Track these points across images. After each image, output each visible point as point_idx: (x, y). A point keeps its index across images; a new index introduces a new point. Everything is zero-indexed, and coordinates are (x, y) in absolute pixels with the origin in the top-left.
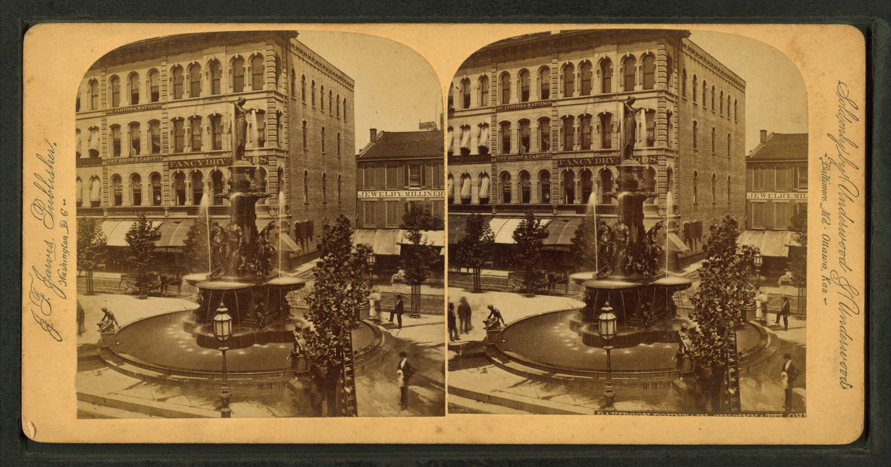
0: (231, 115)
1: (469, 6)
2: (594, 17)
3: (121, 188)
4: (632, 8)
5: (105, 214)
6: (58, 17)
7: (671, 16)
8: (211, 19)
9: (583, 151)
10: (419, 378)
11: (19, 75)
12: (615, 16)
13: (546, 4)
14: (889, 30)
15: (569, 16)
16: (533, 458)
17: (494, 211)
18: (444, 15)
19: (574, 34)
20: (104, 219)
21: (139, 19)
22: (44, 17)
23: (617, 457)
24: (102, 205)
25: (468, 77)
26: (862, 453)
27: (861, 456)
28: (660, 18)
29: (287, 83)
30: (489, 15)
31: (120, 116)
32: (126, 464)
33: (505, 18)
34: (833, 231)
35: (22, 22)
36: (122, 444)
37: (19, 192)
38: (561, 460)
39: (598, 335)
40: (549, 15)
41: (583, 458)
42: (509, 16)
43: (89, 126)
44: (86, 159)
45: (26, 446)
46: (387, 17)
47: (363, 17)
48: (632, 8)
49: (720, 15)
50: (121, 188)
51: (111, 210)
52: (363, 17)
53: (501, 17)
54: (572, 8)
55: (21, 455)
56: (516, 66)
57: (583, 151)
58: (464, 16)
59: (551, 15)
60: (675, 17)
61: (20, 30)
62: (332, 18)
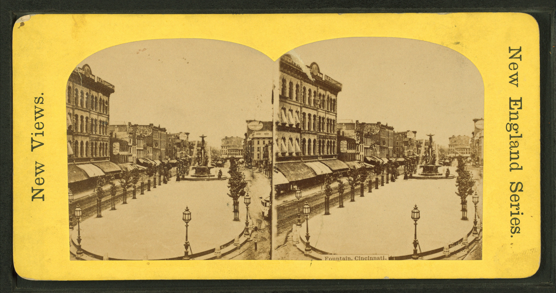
0: (284, 201)
4: (400, 2)
7: (425, 8)
10: (263, 231)
14: (113, 144)
15: (360, 8)
16: (339, 289)
21: (87, 11)
22: (27, 10)
23: (392, 288)
25: (113, 181)
26: (548, 285)
27: (548, 287)
33: (320, 9)
34: (390, 134)
35: (13, 14)
37: (11, 122)
38: (357, 291)
40: (348, 8)
41: (371, 290)
42: (322, 9)
45: (17, 283)
55: (13, 289)
58: (293, 8)
59: (348, 8)
60: (428, 9)
61: (11, 20)
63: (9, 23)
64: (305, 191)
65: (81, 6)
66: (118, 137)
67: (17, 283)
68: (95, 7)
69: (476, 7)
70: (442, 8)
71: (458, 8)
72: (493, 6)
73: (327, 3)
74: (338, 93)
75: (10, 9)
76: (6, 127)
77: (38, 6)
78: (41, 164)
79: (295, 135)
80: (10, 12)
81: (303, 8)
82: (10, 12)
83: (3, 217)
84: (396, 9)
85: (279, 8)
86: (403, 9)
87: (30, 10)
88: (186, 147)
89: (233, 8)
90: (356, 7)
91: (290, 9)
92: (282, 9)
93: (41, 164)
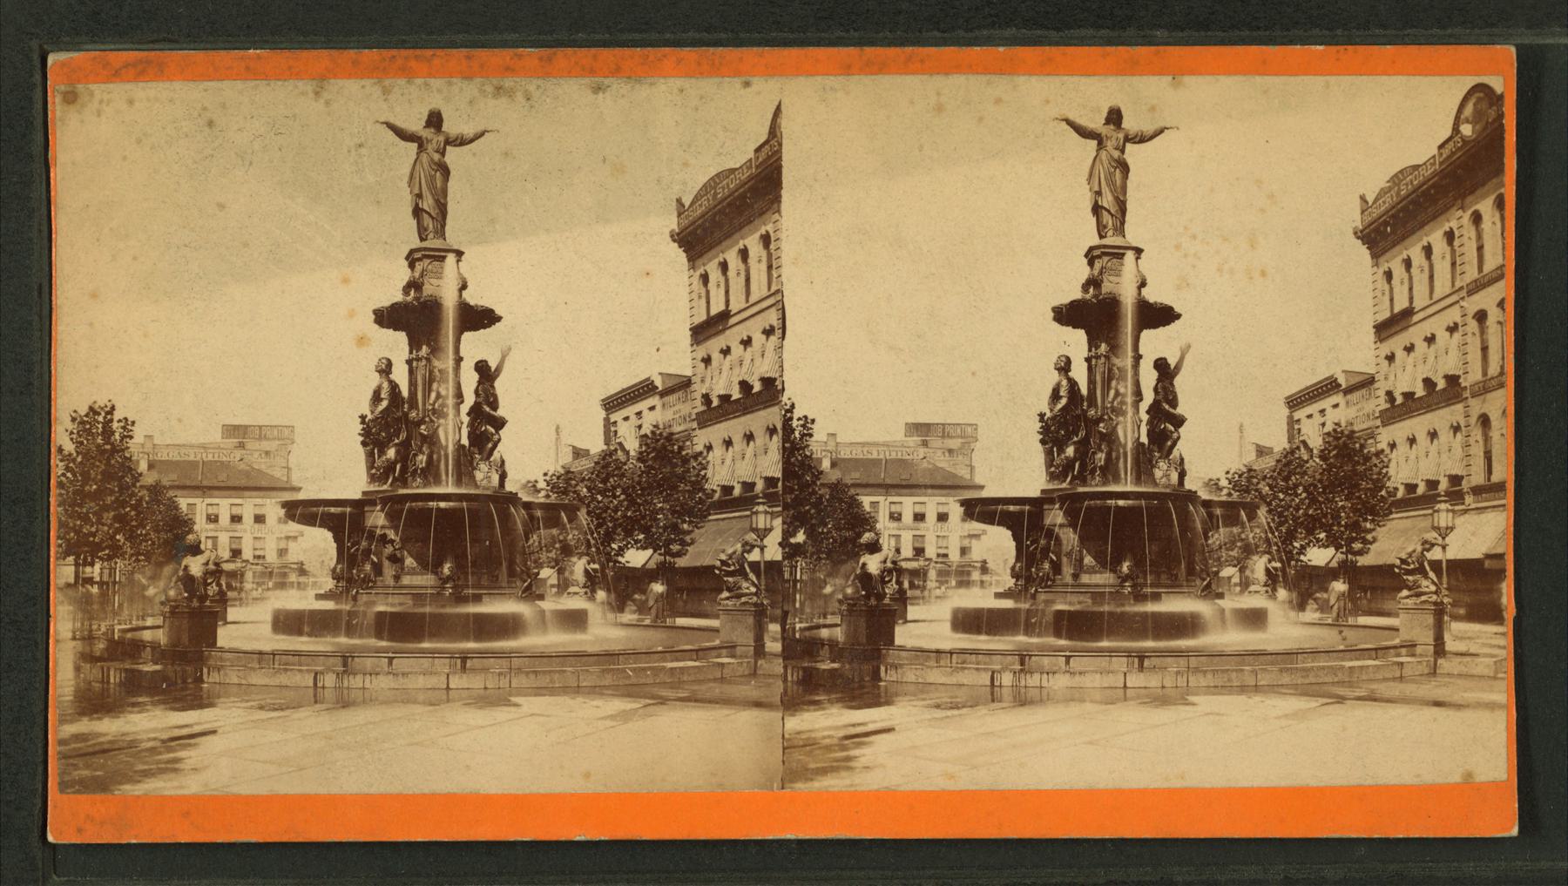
2: (1142, 34)
4: (1213, 13)
5: (1469, 499)
6: (110, 39)
7: (1288, 30)
8: (404, 42)
9: (1122, 251)
11: (37, 149)
17: (1469, 499)
19: (89, 47)
20: (1466, 511)
24: (1465, 485)
29: (695, 674)
30: (938, 30)
32: (1020, 884)
33: (970, 35)
36: (482, 842)
39: (1318, 595)
40: (1054, 29)
46: (742, 35)
47: (697, 36)
48: (1213, 13)
49: (1384, 27)
51: (1477, 491)
52: (697, 36)
53: (961, 33)
54: (1098, 16)
56: (1484, 197)
57: (1122, 251)
59: (1058, 29)
62: (637, 36)
63: (32, 76)
64: (793, 715)
65: (248, 27)
66: (71, 608)
67: (54, 865)
68: (290, 29)
69: (1444, 28)
70: (1339, 32)
72: (1493, 25)
73: (991, 16)
74: (330, 529)
75: (32, 34)
77: (117, 24)
78: (1416, 323)
79: (1442, 418)
80: (34, 44)
81: (920, 32)
82: (34, 44)
83: (13, 663)
84: (1203, 33)
85: (848, 31)
86: (1223, 34)
87: (93, 37)
88: (1452, 415)
89: (707, 30)
90: (1079, 27)
92: (856, 34)
93: (1416, 323)
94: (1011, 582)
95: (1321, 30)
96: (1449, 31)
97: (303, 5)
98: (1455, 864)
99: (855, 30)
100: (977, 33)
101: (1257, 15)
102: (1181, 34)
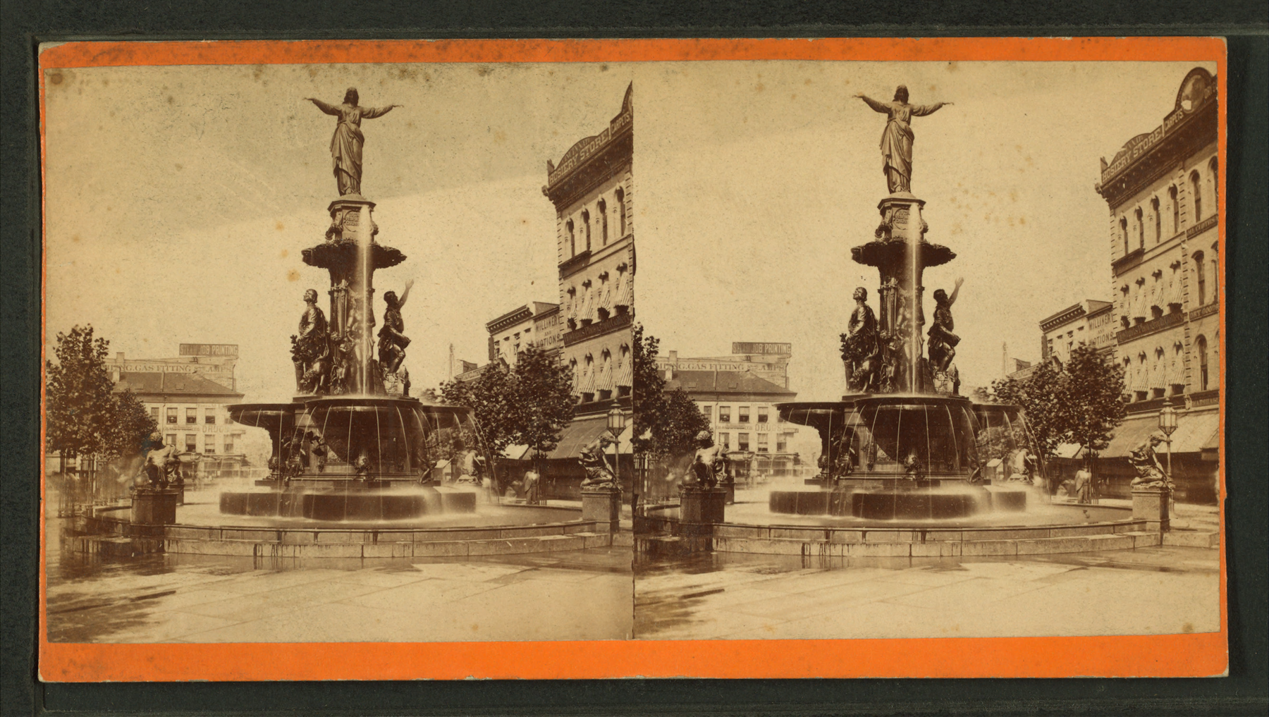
1: (728, 10)
3: (106, 351)
4: (982, 11)
5: (1189, 404)
7: (1042, 24)
8: (327, 34)
9: (908, 203)
12: (957, 24)
13: (803, 10)
15: (883, 26)
18: (689, 25)
21: (215, 34)
28: (438, 30)
30: (759, 24)
31: (1200, 237)
40: (853, 23)
43: (1170, 263)
44: (598, 323)
46: (600, 29)
47: (564, 29)
49: (1120, 22)
50: (106, 351)
51: (1195, 397)
52: (564, 29)
57: (908, 203)
59: (856, 24)
62: (515, 29)
65: (201, 22)
69: (1169, 22)
70: (1084, 26)
71: (1123, 26)
73: (802, 13)
75: (26, 27)
76: (17, 317)
77: (95, 20)
80: (28, 35)
91: (713, 28)
92: (693, 28)
94: (818, 471)
95: (1069, 24)
96: (1173, 25)
97: (749, 4)
98: (1178, 699)
99: (692, 24)
100: (791, 27)
101: (1017, 12)
102: (955, 28)
